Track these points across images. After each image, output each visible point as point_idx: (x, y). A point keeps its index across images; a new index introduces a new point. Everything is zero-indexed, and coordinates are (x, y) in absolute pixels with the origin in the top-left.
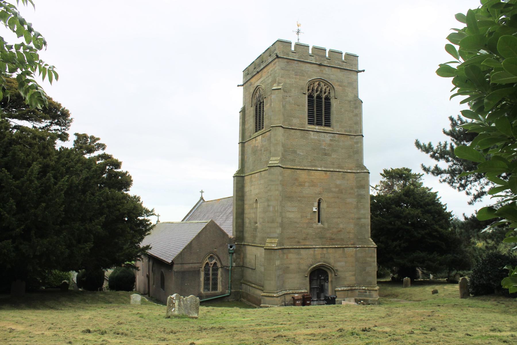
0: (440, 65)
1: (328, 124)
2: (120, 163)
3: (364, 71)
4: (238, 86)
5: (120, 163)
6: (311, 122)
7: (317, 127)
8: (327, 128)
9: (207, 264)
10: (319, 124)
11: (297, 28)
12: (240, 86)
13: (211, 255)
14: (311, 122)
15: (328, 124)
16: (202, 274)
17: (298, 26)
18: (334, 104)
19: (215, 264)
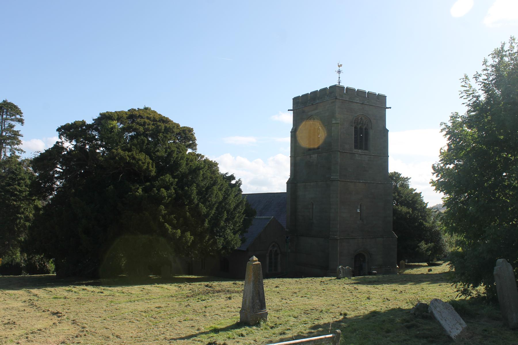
0: (100, 114)
1: (366, 148)
2: (192, 129)
3: (390, 108)
4: (390, 108)
5: (192, 129)
6: (356, 147)
7: (360, 151)
8: (366, 151)
9: (271, 251)
10: (361, 148)
11: (337, 69)
12: (291, 110)
13: (274, 243)
14: (356, 147)
15: (366, 148)
16: (268, 259)
17: (339, 66)
18: (371, 133)
19: (276, 251)
